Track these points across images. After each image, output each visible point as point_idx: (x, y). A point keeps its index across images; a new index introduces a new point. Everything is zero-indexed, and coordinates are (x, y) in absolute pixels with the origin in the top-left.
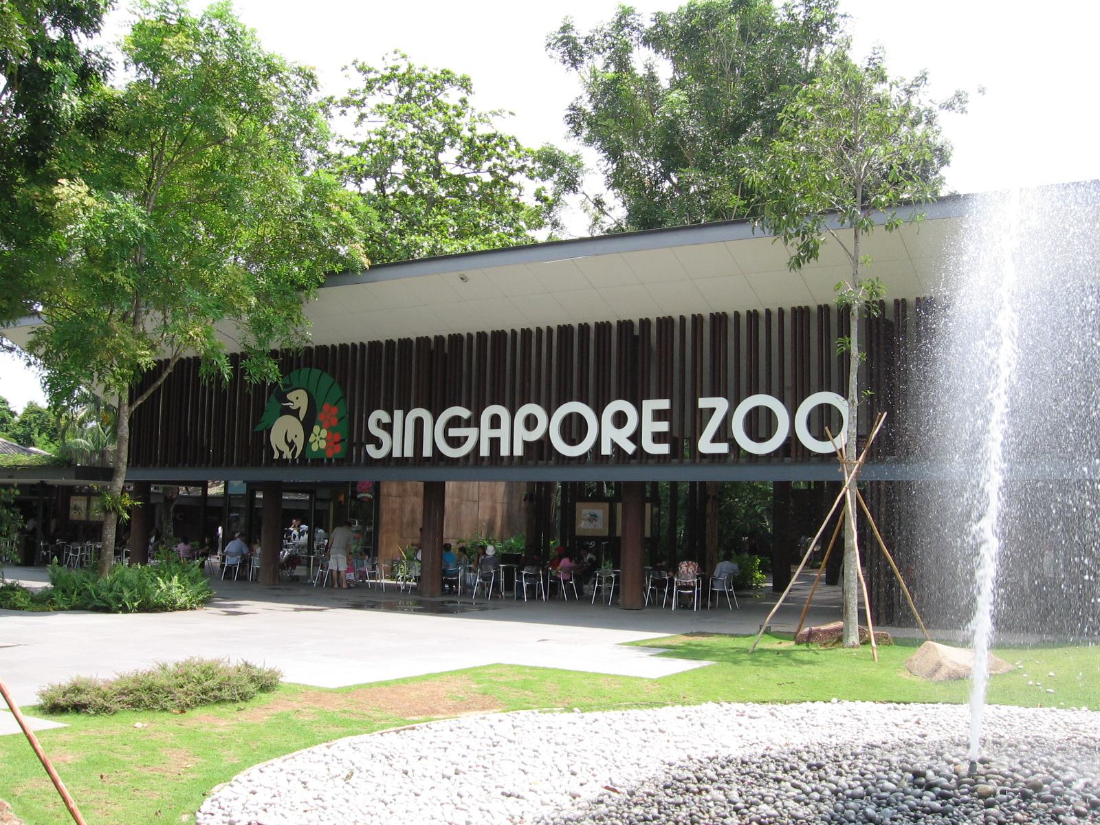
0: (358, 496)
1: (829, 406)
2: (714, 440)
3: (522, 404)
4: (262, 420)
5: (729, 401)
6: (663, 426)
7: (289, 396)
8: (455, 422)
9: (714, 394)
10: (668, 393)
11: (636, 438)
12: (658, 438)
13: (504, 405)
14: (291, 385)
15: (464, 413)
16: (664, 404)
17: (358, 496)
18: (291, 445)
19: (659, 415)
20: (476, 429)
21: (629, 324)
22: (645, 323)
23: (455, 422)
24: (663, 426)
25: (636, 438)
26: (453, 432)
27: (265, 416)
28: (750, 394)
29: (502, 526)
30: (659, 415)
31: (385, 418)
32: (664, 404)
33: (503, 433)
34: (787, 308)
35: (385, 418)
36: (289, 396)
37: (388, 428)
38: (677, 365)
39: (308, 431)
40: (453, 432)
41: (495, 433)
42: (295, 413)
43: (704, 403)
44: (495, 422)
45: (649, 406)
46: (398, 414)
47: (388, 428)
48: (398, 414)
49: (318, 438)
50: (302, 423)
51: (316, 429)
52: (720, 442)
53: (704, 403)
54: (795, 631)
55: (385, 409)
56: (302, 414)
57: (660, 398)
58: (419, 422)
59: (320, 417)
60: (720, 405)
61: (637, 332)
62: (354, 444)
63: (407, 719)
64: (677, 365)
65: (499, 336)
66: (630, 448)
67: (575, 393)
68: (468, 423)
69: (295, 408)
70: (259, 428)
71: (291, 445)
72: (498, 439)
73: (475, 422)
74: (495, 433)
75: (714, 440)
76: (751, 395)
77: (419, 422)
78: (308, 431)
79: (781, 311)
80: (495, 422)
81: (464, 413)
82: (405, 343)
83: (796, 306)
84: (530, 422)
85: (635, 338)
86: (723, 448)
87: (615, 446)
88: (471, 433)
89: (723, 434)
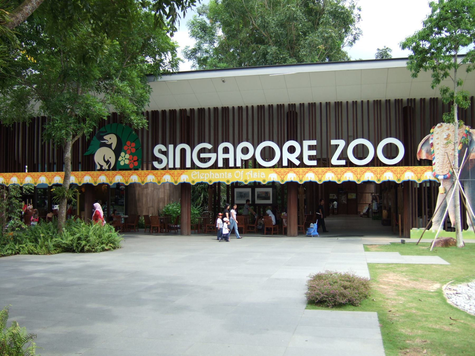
0: (120, 188)
1: (363, 145)
2: (339, 159)
3: (239, 143)
4: (88, 149)
5: (345, 141)
6: (314, 153)
7: (105, 137)
8: (203, 150)
9: (337, 138)
10: (295, 138)
11: (300, 158)
12: (311, 158)
13: (297, 141)
14: (106, 132)
15: (209, 146)
16: (314, 143)
17: (120, 188)
18: (107, 162)
19: (311, 148)
20: (215, 154)
21: (185, 110)
22: (192, 110)
23: (203, 150)
24: (314, 153)
25: (300, 158)
26: (202, 155)
27: (90, 148)
28: (199, 143)
29: (167, 200)
30: (311, 148)
31: (164, 149)
32: (314, 143)
33: (230, 156)
34: (255, 105)
35: (164, 149)
36: (105, 137)
37: (165, 153)
38: (372, 123)
39: (117, 155)
40: (202, 155)
41: (226, 156)
42: (110, 146)
43: (333, 142)
44: (226, 150)
45: (306, 143)
46: (171, 147)
47: (165, 153)
48: (171, 147)
49: (124, 159)
50: (114, 151)
51: (123, 154)
52: (341, 160)
53: (333, 142)
54: (417, 241)
55: (163, 144)
56: (114, 146)
57: (313, 140)
58: (183, 151)
59: (125, 148)
60: (341, 143)
61: (188, 114)
62: (80, 163)
63: (453, 281)
64: (372, 123)
65: (225, 110)
66: (297, 163)
67: (160, 140)
68: (209, 151)
69: (109, 143)
70: (87, 153)
71: (107, 162)
72: (228, 159)
73: (215, 150)
74: (226, 156)
75: (339, 159)
76: (199, 144)
77: (183, 151)
78: (117, 155)
79: (253, 106)
80: (226, 150)
81: (209, 146)
82: (173, 112)
83: (259, 105)
84: (245, 151)
85: (188, 117)
86: (343, 162)
87: (289, 161)
88: (213, 156)
89: (343, 156)
